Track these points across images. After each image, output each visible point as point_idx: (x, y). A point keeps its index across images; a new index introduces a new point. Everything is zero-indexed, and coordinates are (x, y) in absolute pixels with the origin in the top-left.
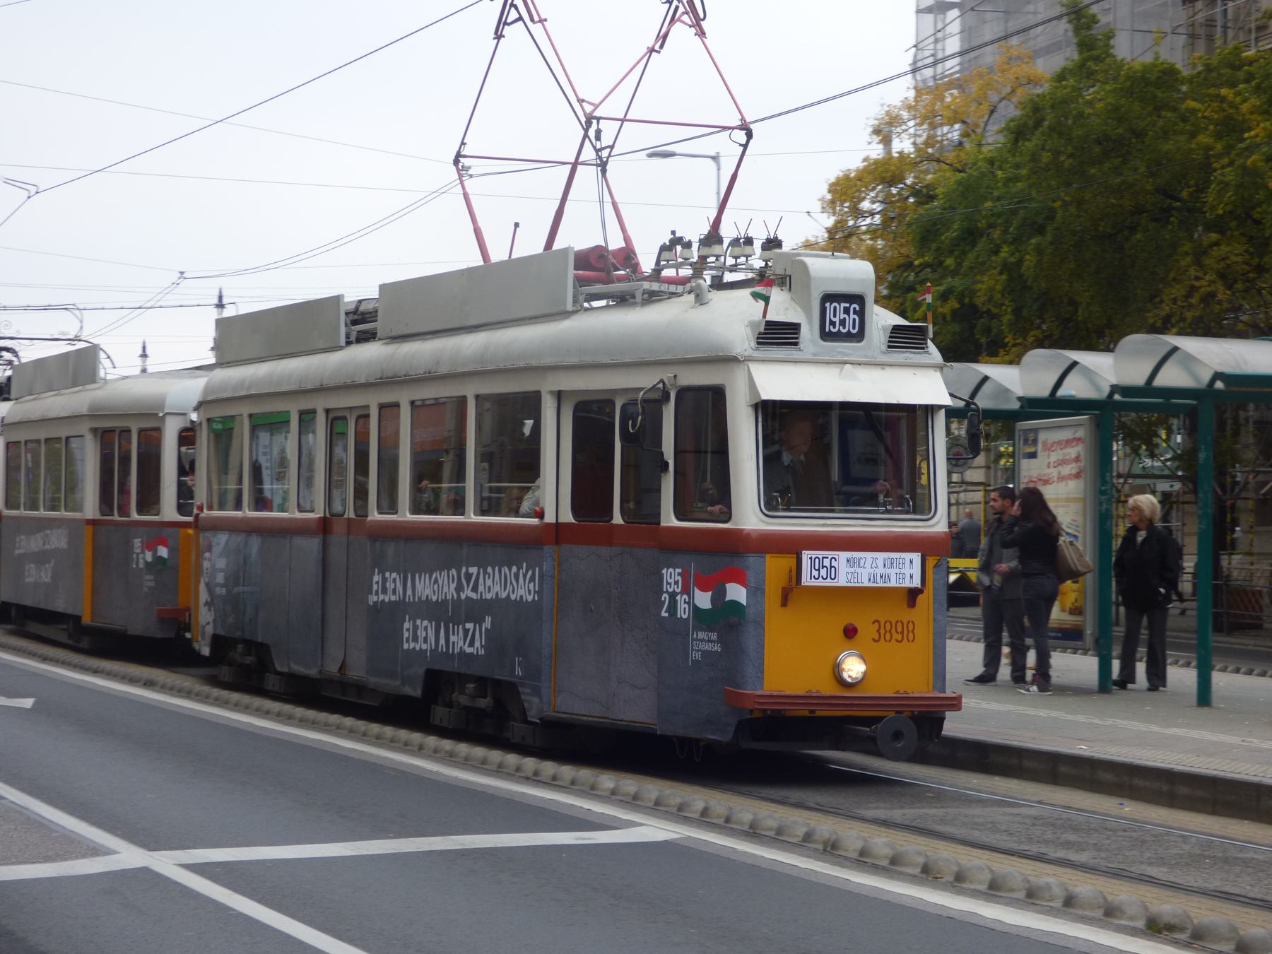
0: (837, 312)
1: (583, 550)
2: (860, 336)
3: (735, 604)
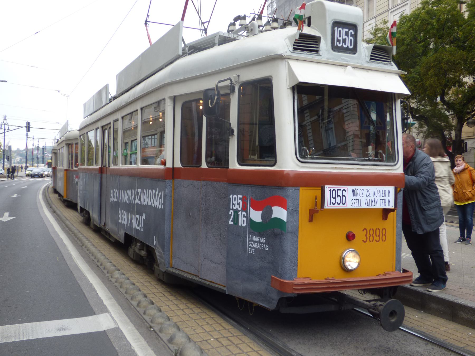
0: (341, 33)
1: (185, 183)
2: (354, 50)
3: (279, 221)
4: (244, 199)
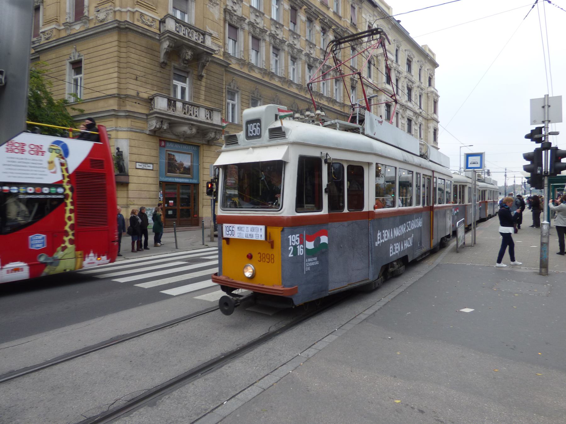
4: (301, 237)
